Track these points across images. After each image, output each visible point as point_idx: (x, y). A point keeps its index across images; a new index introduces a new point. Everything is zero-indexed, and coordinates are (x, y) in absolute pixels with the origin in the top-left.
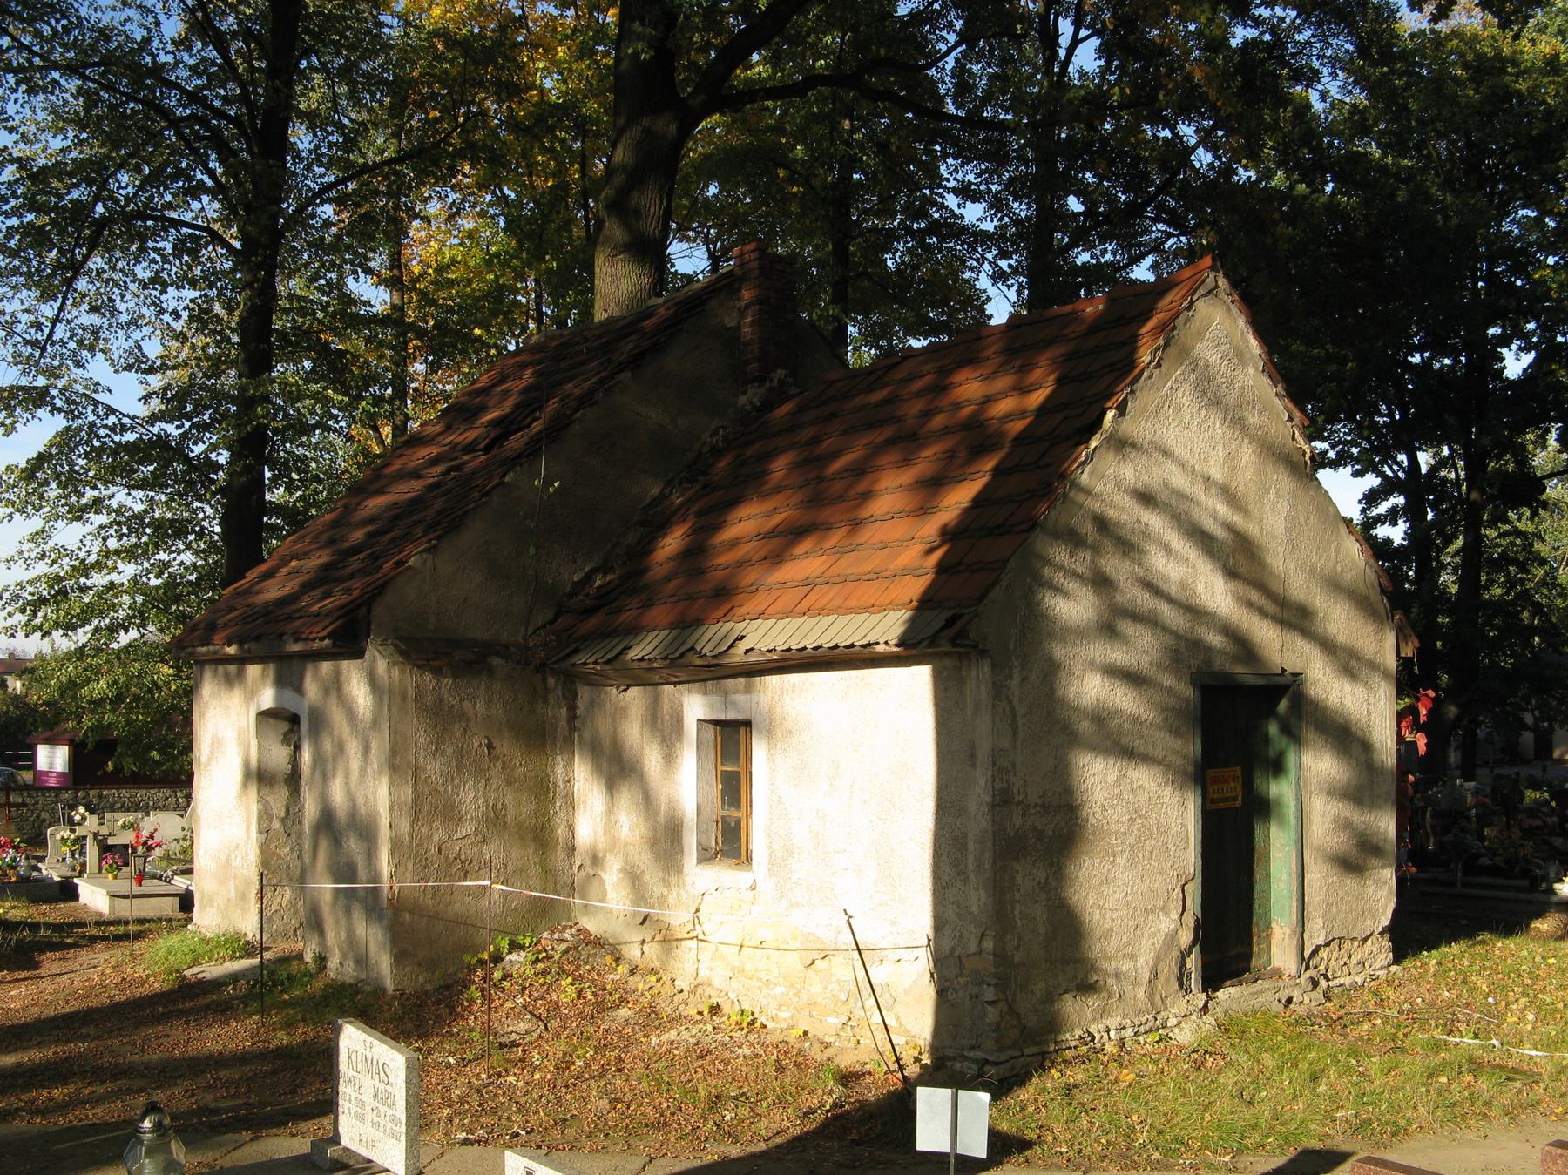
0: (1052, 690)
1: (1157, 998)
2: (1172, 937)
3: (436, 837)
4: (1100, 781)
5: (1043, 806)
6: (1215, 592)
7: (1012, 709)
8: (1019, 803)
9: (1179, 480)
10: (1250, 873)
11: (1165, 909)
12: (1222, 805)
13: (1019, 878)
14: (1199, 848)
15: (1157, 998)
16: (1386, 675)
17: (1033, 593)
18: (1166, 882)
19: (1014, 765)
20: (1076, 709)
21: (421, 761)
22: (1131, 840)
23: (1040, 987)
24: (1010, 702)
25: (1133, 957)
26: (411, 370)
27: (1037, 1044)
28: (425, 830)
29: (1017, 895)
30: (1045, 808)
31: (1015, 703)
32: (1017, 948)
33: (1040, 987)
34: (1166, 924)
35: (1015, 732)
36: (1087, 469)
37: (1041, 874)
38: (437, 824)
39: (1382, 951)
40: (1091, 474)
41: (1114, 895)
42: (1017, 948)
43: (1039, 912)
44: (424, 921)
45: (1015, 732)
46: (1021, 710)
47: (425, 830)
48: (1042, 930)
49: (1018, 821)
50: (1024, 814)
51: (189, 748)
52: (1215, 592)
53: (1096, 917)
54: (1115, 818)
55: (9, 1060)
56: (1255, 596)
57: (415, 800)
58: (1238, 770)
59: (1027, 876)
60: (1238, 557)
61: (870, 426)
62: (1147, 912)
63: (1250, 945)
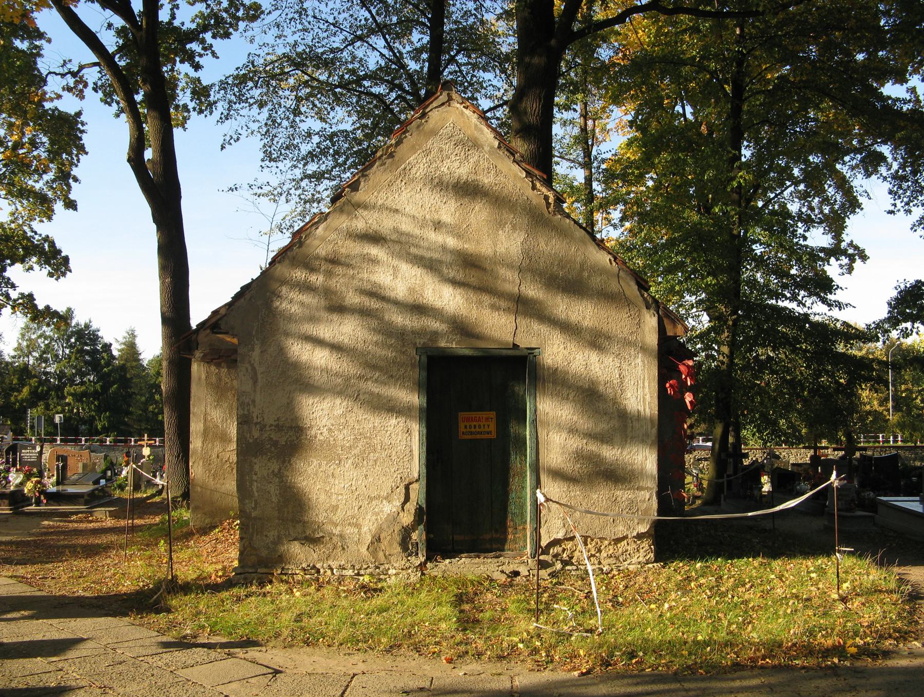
1: (381, 554)
2: (394, 518)
3: (216, 450)
4: (322, 414)
5: (277, 426)
7: (254, 369)
8: (256, 424)
9: (406, 226)
10: (505, 484)
11: (388, 498)
12: (478, 437)
13: (256, 468)
15: (381, 554)
16: (644, 349)
19: (254, 401)
20: (316, 369)
21: (208, 409)
22: (356, 451)
23: (272, 534)
26: (751, 176)
27: (266, 567)
28: (210, 446)
30: (279, 428)
31: (255, 365)
33: (272, 534)
34: (389, 508)
35: (255, 382)
37: (275, 466)
38: (217, 443)
40: (326, 229)
43: (273, 489)
44: (209, 492)
45: (255, 382)
46: (260, 370)
47: (210, 446)
48: (275, 499)
50: (261, 430)
53: (323, 497)
54: (341, 437)
55: (4, 539)
57: (205, 430)
58: (493, 414)
59: (262, 467)
62: (371, 499)
63: (505, 533)
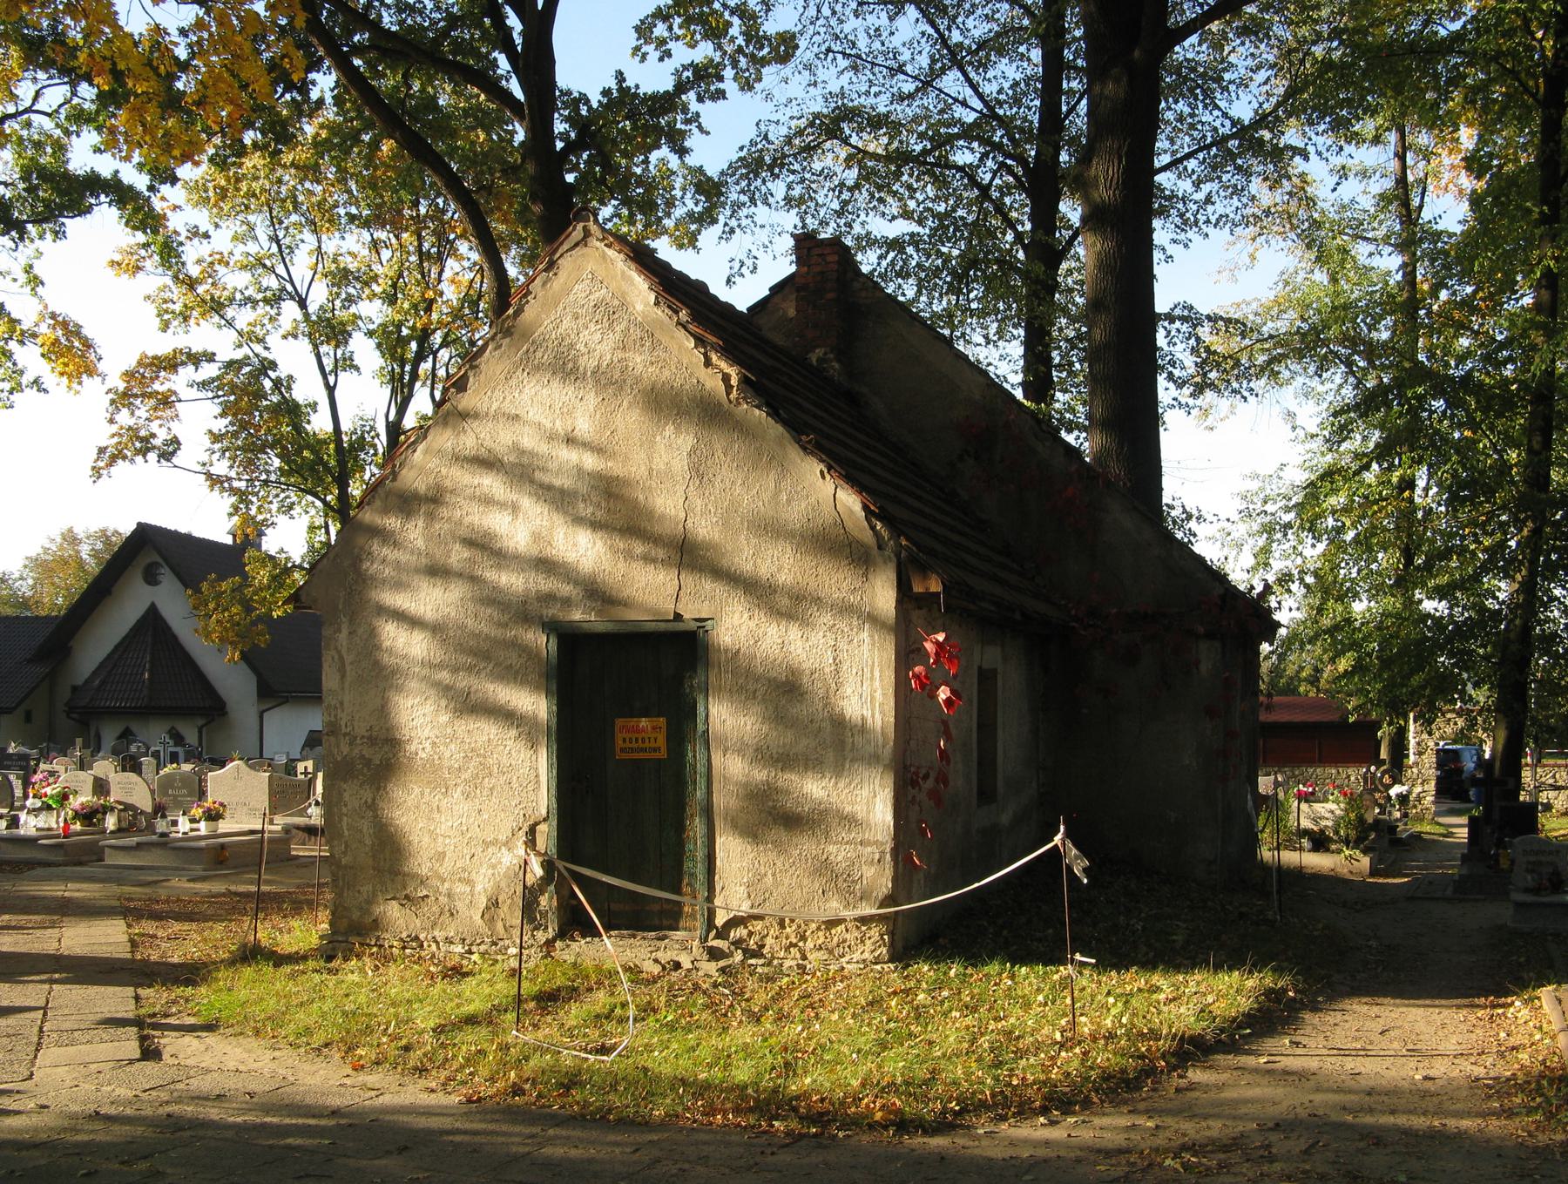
0: (376, 663)
5: (370, 738)
6: (585, 550)
7: (341, 658)
8: (345, 735)
9: (529, 441)
13: (346, 796)
14: (553, 791)
17: (1548, 840)
18: (507, 822)
19: (342, 703)
22: (466, 775)
24: (339, 652)
25: (469, 882)
29: (344, 810)
30: (372, 741)
31: (344, 652)
32: (345, 853)
33: (366, 889)
35: (343, 677)
36: (421, 448)
37: (367, 795)
39: (870, 946)
41: (445, 824)
42: (345, 853)
43: (365, 826)
45: (343, 677)
46: (348, 659)
48: (368, 842)
49: (345, 750)
51: (169, 629)
52: (585, 550)
54: (447, 754)
56: (639, 548)
60: (615, 508)
61: (1222, 1104)
62: (487, 844)
